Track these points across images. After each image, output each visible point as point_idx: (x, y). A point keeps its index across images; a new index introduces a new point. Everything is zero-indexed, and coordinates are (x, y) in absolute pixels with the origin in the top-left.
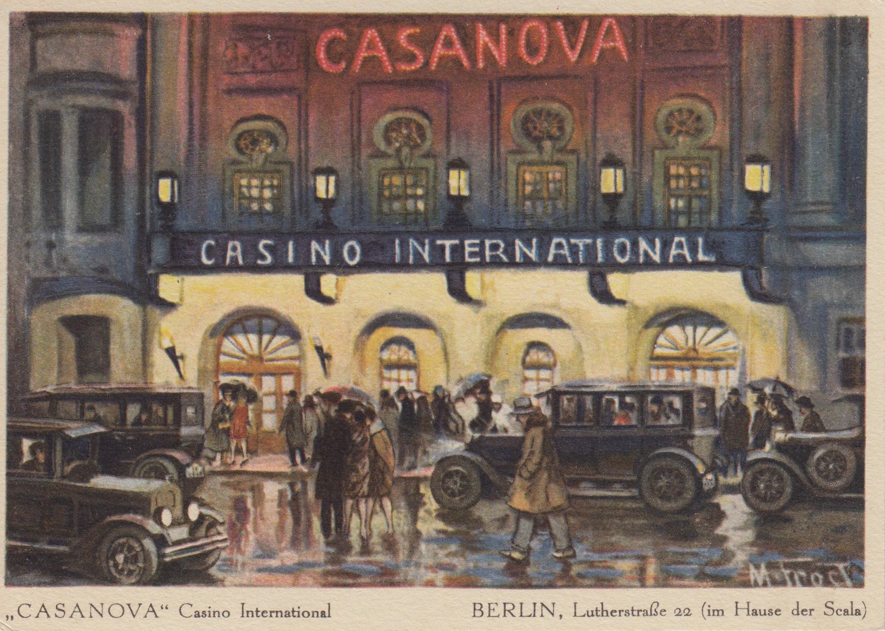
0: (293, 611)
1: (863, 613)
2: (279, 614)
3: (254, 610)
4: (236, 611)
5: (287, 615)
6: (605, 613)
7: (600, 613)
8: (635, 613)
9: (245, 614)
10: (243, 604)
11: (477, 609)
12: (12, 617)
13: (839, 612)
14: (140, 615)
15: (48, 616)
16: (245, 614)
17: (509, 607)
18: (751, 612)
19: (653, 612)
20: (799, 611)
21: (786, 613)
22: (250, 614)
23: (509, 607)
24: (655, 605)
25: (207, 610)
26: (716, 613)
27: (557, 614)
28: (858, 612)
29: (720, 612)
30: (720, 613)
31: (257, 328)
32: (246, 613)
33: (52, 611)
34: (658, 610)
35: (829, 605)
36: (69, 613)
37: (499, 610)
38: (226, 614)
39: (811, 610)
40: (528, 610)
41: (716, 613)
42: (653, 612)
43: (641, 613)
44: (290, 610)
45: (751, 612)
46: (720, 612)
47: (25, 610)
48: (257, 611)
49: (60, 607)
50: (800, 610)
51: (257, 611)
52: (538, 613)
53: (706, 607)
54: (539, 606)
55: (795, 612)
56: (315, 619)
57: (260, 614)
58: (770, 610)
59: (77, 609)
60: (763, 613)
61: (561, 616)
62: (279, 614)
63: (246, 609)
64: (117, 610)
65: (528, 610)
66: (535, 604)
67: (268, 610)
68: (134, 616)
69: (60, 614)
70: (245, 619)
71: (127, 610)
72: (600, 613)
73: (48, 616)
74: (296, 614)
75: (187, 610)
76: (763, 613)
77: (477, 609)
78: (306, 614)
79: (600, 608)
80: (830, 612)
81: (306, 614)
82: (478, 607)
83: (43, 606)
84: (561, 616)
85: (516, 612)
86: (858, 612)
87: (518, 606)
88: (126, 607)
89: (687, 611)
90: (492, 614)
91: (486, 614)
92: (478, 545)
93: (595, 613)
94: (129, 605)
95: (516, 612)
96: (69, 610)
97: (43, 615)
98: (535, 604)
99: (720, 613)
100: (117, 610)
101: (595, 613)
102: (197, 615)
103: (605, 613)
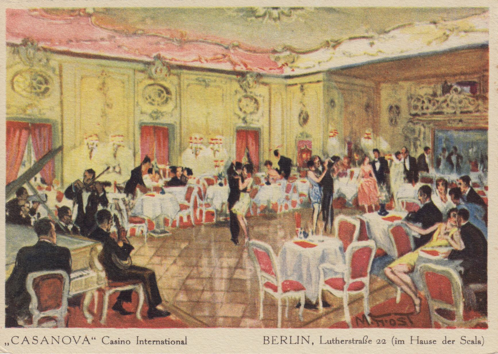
0: (166, 341)
1: (482, 343)
2: (158, 342)
3: (144, 340)
4: (134, 341)
5: (163, 343)
6: (337, 342)
7: (335, 342)
8: (355, 342)
9: (139, 342)
10: (138, 337)
11: (266, 339)
12: (8, 344)
13: (469, 342)
14: (79, 344)
15: (29, 343)
16: (139, 342)
17: (284, 338)
18: (419, 342)
19: (365, 341)
20: (446, 342)
21: (439, 342)
22: (142, 342)
23: (284, 338)
24: (366, 338)
25: (118, 340)
26: (400, 342)
27: (311, 342)
28: (479, 342)
29: (402, 342)
30: (402, 342)
31: (480, 53)
32: (140, 342)
33: (30, 340)
34: (367, 340)
35: (463, 338)
36: (40, 342)
37: (278, 340)
38: (128, 342)
39: (453, 341)
40: (294, 340)
41: (400, 342)
42: (365, 341)
43: (358, 342)
44: (164, 340)
45: (419, 342)
46: (402, 342)
47: (15, 340)
48: (146, 341)
49: (35, 338)
50: (447, 341)
51: (146, 341)
52: (300, 342)
53: (394, 340)
54: (300, 338)
55: (444, 342)
56: (178, 345)
57: (147, 342)
58: (430, 341)
59: (25, 340)
60: (426, 342)
61: (313, 343)
62: (158, 342)
63: (139, 339)
64: (67, 340)
65: (294, 340)
66: (298, 337)
67: (152, 340)
68: (76, 343)
69: (35, 342)
70: (139, 345)
71: (73, 339)
72: (335, 342)
73: (29, 343)
74: (167, 342)
75: (106, 340)
76: (426, 342)
77: (266, 339)
78: (173, 343)
79: (335, 339)
80: (463, 342)
81: (173, 343)
82: (266, 338)
83: (26, 337)
84: (313, 343)
85: (288, 341)
86: (479, 342)
87: (289, 338)
88: (72, 338)
89: (383, 341)
90: (274, 343)
91: (271, 342)
92: (11, 135)
93: (332, 342)
94: (291, 337)
95: (288, 341)
96: (40, 339)
97: (26, 343)
98: (298, 337)
99: (402, 342)
100: (67, 340)
101: (332, 342)
102: (112, 343)
103: (337, 342)
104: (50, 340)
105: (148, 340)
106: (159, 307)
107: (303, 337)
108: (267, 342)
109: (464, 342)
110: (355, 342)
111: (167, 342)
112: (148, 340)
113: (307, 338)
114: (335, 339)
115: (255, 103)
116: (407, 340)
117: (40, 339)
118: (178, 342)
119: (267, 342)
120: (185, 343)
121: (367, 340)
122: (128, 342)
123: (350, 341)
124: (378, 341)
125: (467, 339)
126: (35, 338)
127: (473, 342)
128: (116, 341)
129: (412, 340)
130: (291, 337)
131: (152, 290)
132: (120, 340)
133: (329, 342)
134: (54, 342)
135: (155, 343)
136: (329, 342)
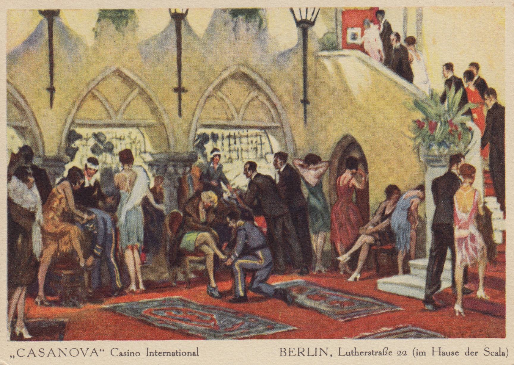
1: (506, 354)
2: (169, 354)
5: (173, 354)
6: (357, 354)
7: (354, 354)
8: (374, 353)
9: (149, 354)
11: (283, 352)
12: (14, 356)
13: (493, 354)
14: (87, 356)
16: (149, 354)
17: (301, 350)
18: (441, 354)
19: (385, 353)
20: (469, 353)
22: (152, 354)
23: (301, 350)
25: (127, 352)
26: (421, 353)
28: (503, 354)
29: (423, 353)
32: (149, 354)
34: (388, 352)
36: (46, 355)
37: (296, 352)
38: (138, 354)
39: (476, 352)
40: (312, 352)
41: (421, 353)
42: (385, 353)
43: (378, 354)
44: (175, 352)
45: (441, 354)
46: (423, 353)
47: (21, 353)
48: (156, 352)
51: (156, 352)
52: (318, 353)
53: (415, 351)
54: (318, 350)
55: (467, 354)
57: (157, 354)
58: (452, 353)
61: (331, 355)
64: (74, 352)
65: (312, 352)
66: (316, 348)
68: (84, 356)
69: (42, 354)
70: (149, 356)
71: (80, 351)
72: (354, 354)
74: (178, 354)
75: (115, 352)
79: (354, 351)
80: (487, 353)
81: (184, 354)
82: (283, 350)
84: (331, 355)
85: (305, 353)
87: (306, 350)
89: (404, 353)
91: (288, 354)
94: (308, 348)
95: (305, 353)
96: (47, 352)
97: (32, 355)
98: (316, 348)
100: (74, 352)
102: (121, 354)
103: (357, 354)
104: (56, 352)
105: (158, 352)
106: (117, 74)
107: (321, 349)
108: (283, 354)
109: (488, 353)
110: (374, 353)
111: (178, 354)
112: (158, 352)
113: (325, 350)
114: (354, 351)
115: (248, 21)
116: (429, 352)
117: (47, 352)
118: (190, 354)
119: (283, 354)
120: (196, 354)
121: (388, 352)
122: (138, 354)
123: (370, 353)
124: (399, 353)
125: (490, 351)
126: (41, 350)
127: (497, 354)
128: (125, 353)
129: (433, 351)
130: (308, 348)
131: (440, 270)
132: (129, 352)
133: (348, 354)
134: (61, 354)
135: (166, 354)
136: (348, 354)
